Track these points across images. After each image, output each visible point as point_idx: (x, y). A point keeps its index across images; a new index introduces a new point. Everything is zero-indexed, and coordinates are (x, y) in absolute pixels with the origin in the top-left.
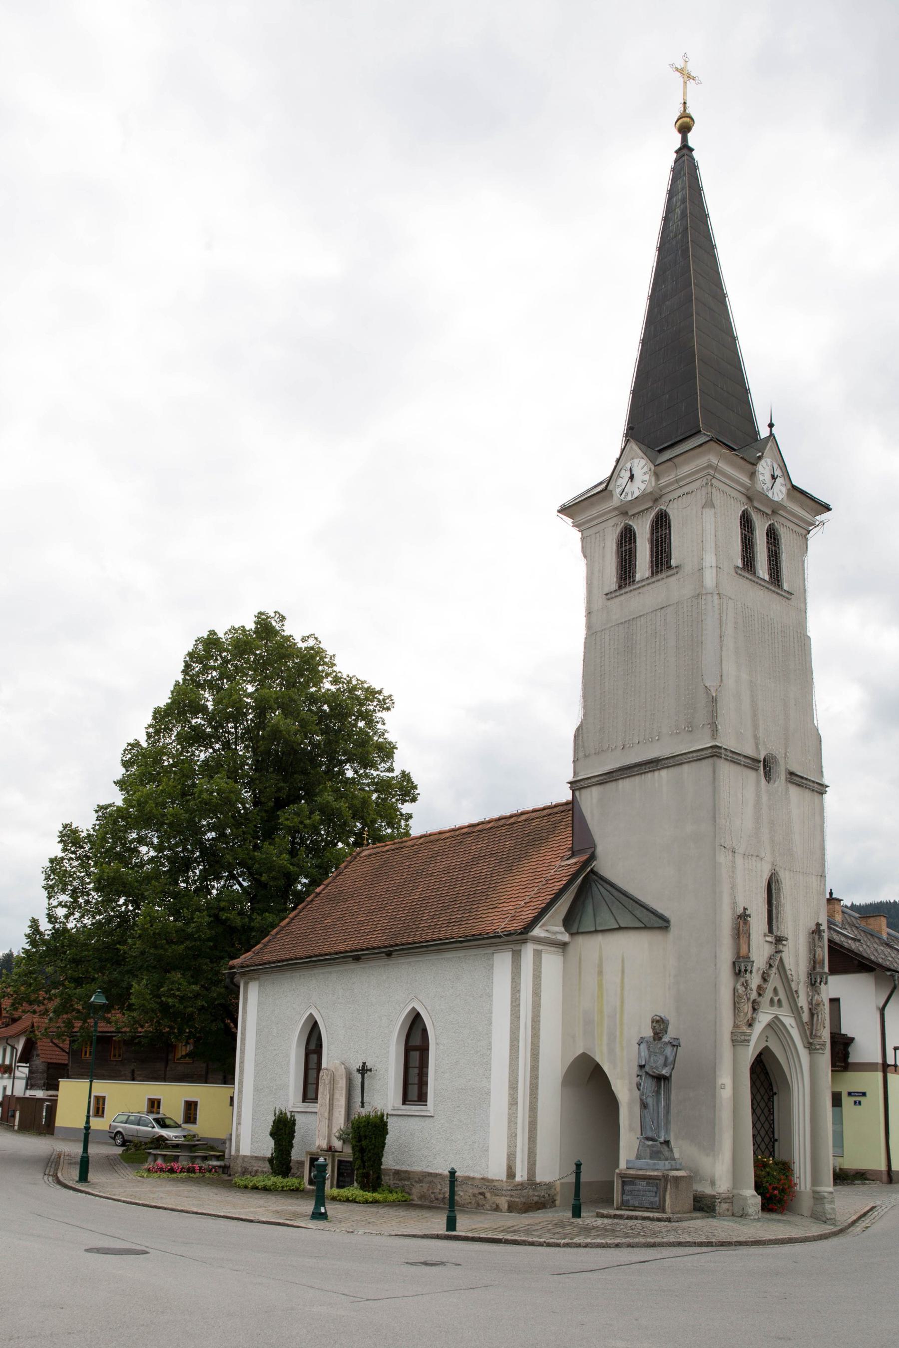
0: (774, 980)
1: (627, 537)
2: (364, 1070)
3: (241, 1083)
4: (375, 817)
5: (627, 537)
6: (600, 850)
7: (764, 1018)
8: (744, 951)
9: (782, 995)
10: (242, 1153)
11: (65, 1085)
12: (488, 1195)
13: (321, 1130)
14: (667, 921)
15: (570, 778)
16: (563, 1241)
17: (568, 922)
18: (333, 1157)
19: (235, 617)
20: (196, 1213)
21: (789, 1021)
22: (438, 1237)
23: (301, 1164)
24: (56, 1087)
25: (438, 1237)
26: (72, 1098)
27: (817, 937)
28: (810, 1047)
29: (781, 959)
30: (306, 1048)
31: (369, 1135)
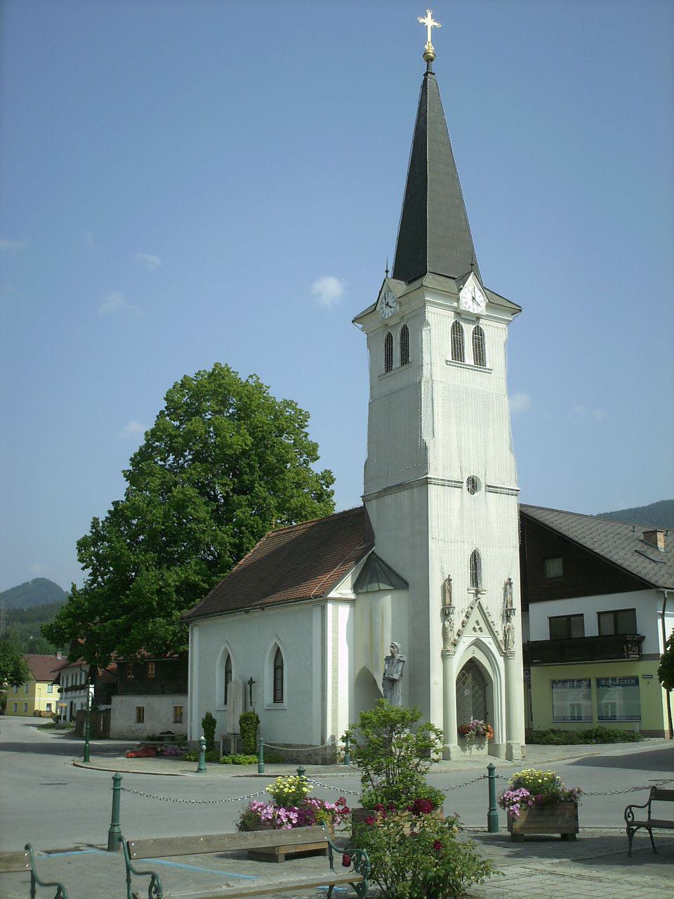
0: (476, 615)
1: (389, 339)
2: (251, 682)
3: (191, 694)
4: (274, 511)
5: (389, 339)
6: (377, 540)
7: (467, 640)
8: (448, 602)
9: (483, 625)
10: (193, 739)
11: (116, 700)
12: (313, 755)
13: (229, 724)
14: (408, 584)
15: (362, 494)
16: (312, 775)
17: (356, 587)
18: (235, 737)
19: (196, 364)
20: (137, 773)
21: (488, 640)
22: (255, 776)
23: (219, 743)
24: (109, 702)
25: (255, 776)
26: (123, 709)
27: (508, 587)
28: (506, 656)
29: (479, 603)
30: (275, 665)
31: (249, 722)
